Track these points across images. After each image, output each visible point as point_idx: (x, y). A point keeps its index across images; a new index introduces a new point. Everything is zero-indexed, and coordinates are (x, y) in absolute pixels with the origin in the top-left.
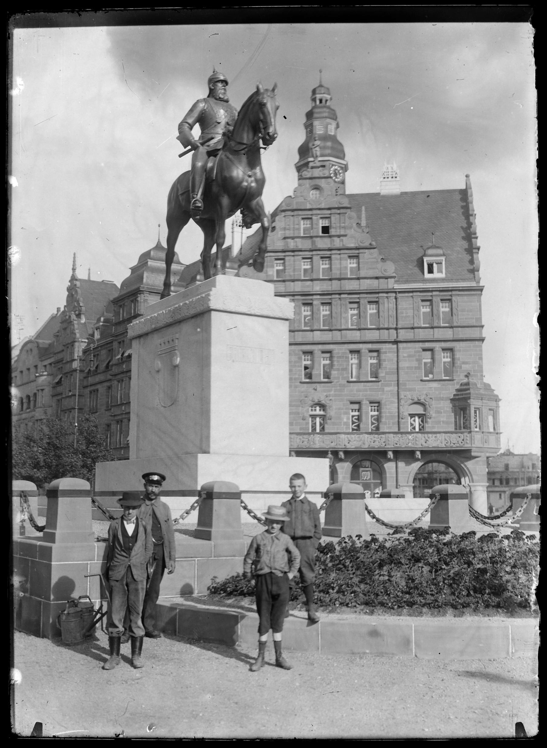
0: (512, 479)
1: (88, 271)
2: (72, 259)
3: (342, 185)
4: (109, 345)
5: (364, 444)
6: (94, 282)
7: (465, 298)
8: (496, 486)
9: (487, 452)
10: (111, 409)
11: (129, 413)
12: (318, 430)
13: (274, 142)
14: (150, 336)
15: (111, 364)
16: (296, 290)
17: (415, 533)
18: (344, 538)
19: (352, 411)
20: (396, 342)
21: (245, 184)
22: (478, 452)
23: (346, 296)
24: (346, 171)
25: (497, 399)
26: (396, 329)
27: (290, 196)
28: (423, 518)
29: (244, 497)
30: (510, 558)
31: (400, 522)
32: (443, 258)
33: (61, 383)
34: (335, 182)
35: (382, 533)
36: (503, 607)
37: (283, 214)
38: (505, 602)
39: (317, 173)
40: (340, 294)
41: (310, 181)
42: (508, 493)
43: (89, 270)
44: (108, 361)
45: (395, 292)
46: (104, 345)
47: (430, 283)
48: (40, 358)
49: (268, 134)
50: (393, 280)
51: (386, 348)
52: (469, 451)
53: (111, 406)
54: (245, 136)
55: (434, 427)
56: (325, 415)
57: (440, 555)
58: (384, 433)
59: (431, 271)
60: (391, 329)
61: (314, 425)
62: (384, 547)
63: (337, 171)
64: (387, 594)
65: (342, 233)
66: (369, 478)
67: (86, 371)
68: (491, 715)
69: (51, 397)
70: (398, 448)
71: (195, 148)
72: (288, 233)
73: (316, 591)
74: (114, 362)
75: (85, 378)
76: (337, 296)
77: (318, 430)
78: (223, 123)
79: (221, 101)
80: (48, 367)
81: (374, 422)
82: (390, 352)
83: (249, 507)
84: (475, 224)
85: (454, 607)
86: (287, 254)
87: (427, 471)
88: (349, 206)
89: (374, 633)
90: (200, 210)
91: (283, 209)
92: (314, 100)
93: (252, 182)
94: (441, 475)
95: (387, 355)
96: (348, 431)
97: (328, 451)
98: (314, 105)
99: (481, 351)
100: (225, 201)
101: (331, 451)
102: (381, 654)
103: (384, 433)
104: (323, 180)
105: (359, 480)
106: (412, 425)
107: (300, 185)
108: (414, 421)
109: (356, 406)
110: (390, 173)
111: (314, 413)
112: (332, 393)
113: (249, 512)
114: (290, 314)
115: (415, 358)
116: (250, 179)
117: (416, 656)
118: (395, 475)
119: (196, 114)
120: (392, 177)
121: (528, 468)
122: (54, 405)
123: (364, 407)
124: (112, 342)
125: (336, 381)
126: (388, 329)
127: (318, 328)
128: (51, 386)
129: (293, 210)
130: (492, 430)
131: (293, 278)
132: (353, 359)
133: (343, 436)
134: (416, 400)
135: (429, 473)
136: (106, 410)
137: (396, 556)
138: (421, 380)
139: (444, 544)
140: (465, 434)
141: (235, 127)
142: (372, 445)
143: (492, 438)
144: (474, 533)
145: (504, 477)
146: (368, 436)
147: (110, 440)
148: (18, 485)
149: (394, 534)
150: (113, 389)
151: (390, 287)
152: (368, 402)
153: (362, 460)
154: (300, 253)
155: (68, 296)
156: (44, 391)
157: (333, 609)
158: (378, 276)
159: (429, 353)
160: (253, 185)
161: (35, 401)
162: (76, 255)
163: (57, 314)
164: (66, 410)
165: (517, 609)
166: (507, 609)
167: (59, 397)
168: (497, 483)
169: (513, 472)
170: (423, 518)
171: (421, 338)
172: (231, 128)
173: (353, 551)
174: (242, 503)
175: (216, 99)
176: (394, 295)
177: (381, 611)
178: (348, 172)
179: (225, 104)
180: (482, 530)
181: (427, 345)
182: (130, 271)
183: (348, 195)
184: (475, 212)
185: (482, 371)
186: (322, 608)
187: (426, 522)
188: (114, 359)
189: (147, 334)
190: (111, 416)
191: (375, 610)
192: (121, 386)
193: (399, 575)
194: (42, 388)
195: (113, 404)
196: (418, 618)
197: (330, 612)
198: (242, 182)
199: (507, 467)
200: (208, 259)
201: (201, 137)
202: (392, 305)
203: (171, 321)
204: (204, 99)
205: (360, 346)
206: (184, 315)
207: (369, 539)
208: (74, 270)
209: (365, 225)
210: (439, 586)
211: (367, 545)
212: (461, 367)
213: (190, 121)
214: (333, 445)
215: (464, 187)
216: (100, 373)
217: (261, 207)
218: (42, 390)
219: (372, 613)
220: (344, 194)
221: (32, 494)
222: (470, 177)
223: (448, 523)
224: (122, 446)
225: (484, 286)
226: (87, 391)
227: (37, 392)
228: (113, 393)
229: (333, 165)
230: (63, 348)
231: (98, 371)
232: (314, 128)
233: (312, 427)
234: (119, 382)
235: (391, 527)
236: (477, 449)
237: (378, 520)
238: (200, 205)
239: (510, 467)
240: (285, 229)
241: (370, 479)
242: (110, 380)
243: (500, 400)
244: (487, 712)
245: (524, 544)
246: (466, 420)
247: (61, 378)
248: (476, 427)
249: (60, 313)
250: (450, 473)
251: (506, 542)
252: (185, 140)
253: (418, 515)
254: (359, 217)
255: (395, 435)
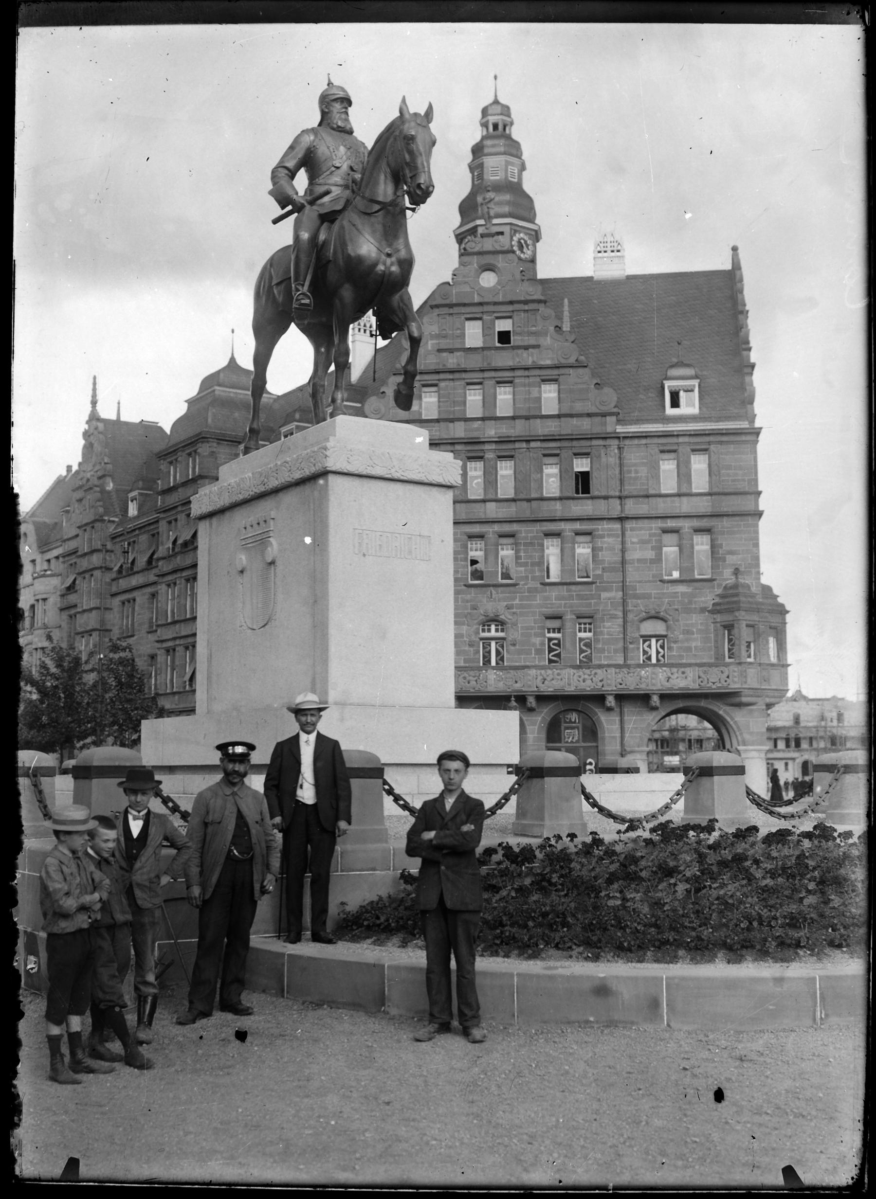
0: (805, 738)
1: (116, 405)
2: (91, 386)
3: (531, 264)
4: (152, 527)
5: (569, 685)
6: (127, 424)
7: (731, 448)
8: (779, 751)
9: (767, 696)
10: (156, 631)
11: (195, 635)
12: (493, 663)
13: (429, 200)
14: (228, 514)
15: (155, 557)
16: (457, 436)
17: (663, 830)
18: (549, 839)
19: (549, 632)
20: (621, 519)
21: (381, 267)
22: (752, 696)
23: (538, 444)
24: (538, 241)
25: (782, 611)
26: (620, 498)
27: (448, 283)
28: (673, 806)
29: (390, 776)
30: (814, 869)
31: (635, 812)
32: (696, 383)
33: (74, 588)
34: (520, 259)
35: (609, 831)
36: (804, 947)
37: (437, 311)
38: (808, 938)
39: (488, 244)
40: (528, 441)
41: (480, 257)
42: (800, 761)
43: (119, 403)
44: (151, 552)
45: (619, 438)
46: (144, 526)
47: (674, 423)
48: (39, 547)
49: (419, 186)
50: (614, 418)
51: (603, 530)
52: (735, 694)
53: (158, 626)
54: (381, 187)
55: (681, 657)
56: (504, 639)
57: (703, 865)
58: (600, 666)
59: (675, 403)
60: (612, 497)
61: (487, 654)
62: (614, 853)
63: (522, 241)
64: (621, 928)
65: (532, 341)
66: (576, 738)
67: (116, 569)
68: (791, 1117)
69: (58, 612)
70: (623, 689)
71: (298, 208)
72: (444, 343)
73: (506, 925)
74: (161, 552)
75: (113, 580)
76: (524, 445)
77: (493, 663)
78: (345, 167)
79: (340, 131)
80: (53, 561)
81: (584, 648)
82: (609, 536)
83: (397, 791)
84: (747, 326)
85: (730, 948)
86: (442, 376)
87: (667, 727)
88: (542, 298)
89: (602, 990)
90: (309, 310)
91: (434, 303)
92: (484, 125)
93: (392, 264)
94: (691, 732)
95: (606, 539)
96: (542, 663)
97: (511, 696)
98: (485, 133)
99: (757, 532)
100: (347, 293)
101: (515, 696)
102: (611, 1024)
103: (600, 666)
104: (500, 256)
105: (560, 742)
106: (645, 652)
107: (462, 264)
108: (650, 646)
109: (556, 624)
110: (609, 245)
111: (486, 635)
112: (517, 602)
113: (397, 798)
114: (455, 478)
115: (650, 545)
116: (389, 261)
117: (668, 1025)
118: (618, 735)
119: (300, 153)
120: (613, 251)
121: (832, 721)
122: (64, 625)
123: (568, 625)
124: (157, 522)
125: (522, 583)
126: (606, 498)
127: (493, 497)
128: (59, 593)
129: (451, 306)
130: (773, 659)
131: (451, 417)
132: (551, 548)
133: (533, 672)
134: (653, 613)
135: (672, 730)
136: (149, 632)
137: (632, 867)
138: (662, 581)
139: (710, 847)
140: (732, 668)
141: (363, 174)
142: (582, 686)
143: (775, 674)
144: (755, 829)
145: (793, 735)
146: (575, 671)
147: (156, 680)
148: (27, 758)
149: (627, 831)
150: (160, 599)
151: (609, 429)
152: (574, 617)
153: (564, 711)
154: (464, 375)
155: (85, 447)
156: (48, 602)
157: (534, 952)
158: (590, 411)
159: (673, 538)
160: (394, 269)
161: (33, 617)
162: (97, 380)
163: (66, 477)
164: (82, 633)
165: (827, 950)
166: (812, 950)
167: (73, 611)
168: (781, 745)
169: (805, 727)
170: (673, 806)
171: (661, 512)
172: (358, 176)
173: (564, 860)
174: (384, 784)
175: (333, 129)
176: (616, 442)
177: (612, 954)
178: (541, 241)
179: (346, 136)
180: (767, 824)
181: (670, 524)
182: (186, 405)
183: (541, 280)
184: (747, 308)
185: (758, 565)
186: (516, 952)
187: (678, 814)
188: (160, 548)
189: (222, 511)
190: (158, 642)
191: (602, 954)
192: (173, 594)
193: (638, 896)
194: (44, 596)
195: (159, 623)
196: (671, 965)
197: (530, 957)
198: (376, 264)
199: (797, 720)
200: (321, 390)
201: (309, 190)
202: (613, 460)
203: (263, 490)
204: (313, 129)
205: (562, 526)
206: (283, 481)
207: (589, 839)
208: (94, 403)
209: (569, 329)
210: (703, 913)
211: (587, 850)
212: (724, 560)
213: (291, 164)
214: (517, 686)
215: (728, 266)
216: (138, 572)
217: (407, 302)
218: (45, 600)
219: (596, 958)
220: (534, 280)
221: (49, 772)
222: (739, 251)
223: (713, 813)
224: (175, 690)
225: (761, 428)
226: (117, 601)
227: (36, 603)
228: (159, 605)
229: (516, 231)
230: (77, 531)
231: (135, 569)
232: (485, 169)
233: (484, 657)
234: (169, 586)
235: (623, 820)
236: (751, 692)
237: (602, 810)
238: (307, 301)
239: (802, 718)
240: (437, 336)
241: (577, 742)
242: (155, 583)
243: (788, 612)
244: (787, 1114)
245: (835, 846)
246: (733, 645)
247: (75, 580)
248: (749, 656)
249: (70, 475)
250: (705, 729)
251: (806, 843)
252: (283, 200)
253: (665, 800)
254: (560, 317)
255: (617, 670)
